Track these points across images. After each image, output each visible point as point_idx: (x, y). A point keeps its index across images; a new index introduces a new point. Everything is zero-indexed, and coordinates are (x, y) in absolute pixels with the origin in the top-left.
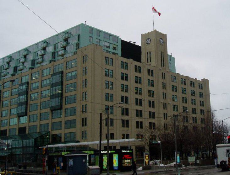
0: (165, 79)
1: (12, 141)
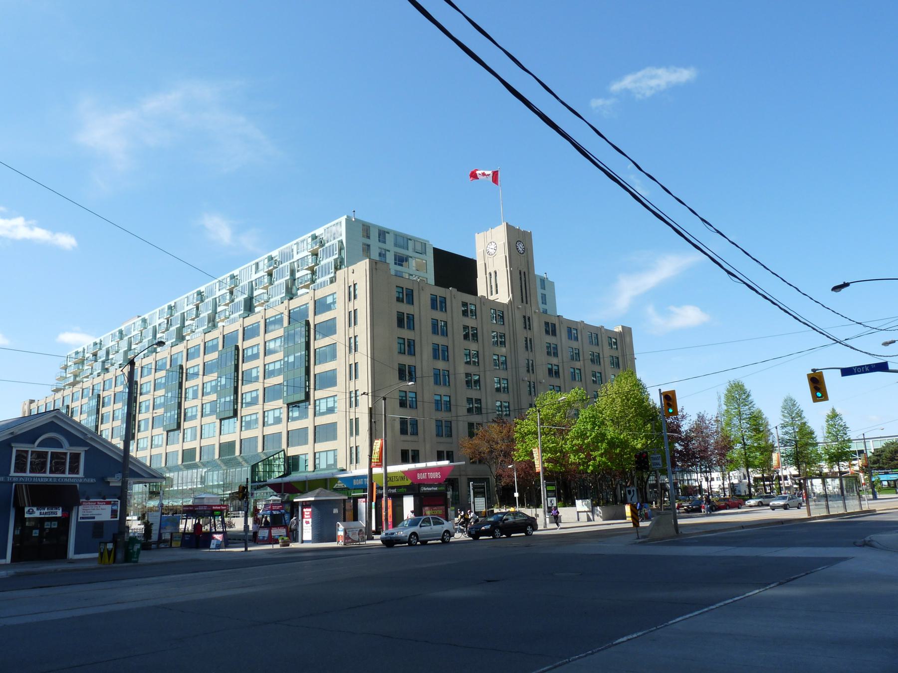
0: (530, 329)
1: (205, 472)
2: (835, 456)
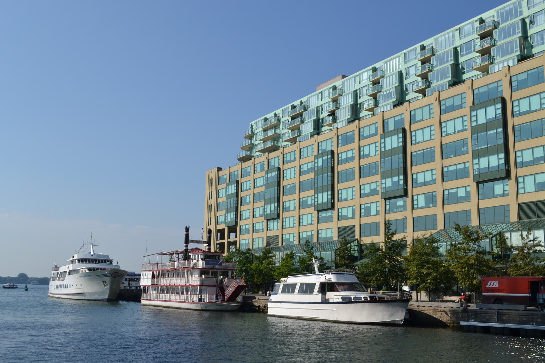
2: (444, 273)
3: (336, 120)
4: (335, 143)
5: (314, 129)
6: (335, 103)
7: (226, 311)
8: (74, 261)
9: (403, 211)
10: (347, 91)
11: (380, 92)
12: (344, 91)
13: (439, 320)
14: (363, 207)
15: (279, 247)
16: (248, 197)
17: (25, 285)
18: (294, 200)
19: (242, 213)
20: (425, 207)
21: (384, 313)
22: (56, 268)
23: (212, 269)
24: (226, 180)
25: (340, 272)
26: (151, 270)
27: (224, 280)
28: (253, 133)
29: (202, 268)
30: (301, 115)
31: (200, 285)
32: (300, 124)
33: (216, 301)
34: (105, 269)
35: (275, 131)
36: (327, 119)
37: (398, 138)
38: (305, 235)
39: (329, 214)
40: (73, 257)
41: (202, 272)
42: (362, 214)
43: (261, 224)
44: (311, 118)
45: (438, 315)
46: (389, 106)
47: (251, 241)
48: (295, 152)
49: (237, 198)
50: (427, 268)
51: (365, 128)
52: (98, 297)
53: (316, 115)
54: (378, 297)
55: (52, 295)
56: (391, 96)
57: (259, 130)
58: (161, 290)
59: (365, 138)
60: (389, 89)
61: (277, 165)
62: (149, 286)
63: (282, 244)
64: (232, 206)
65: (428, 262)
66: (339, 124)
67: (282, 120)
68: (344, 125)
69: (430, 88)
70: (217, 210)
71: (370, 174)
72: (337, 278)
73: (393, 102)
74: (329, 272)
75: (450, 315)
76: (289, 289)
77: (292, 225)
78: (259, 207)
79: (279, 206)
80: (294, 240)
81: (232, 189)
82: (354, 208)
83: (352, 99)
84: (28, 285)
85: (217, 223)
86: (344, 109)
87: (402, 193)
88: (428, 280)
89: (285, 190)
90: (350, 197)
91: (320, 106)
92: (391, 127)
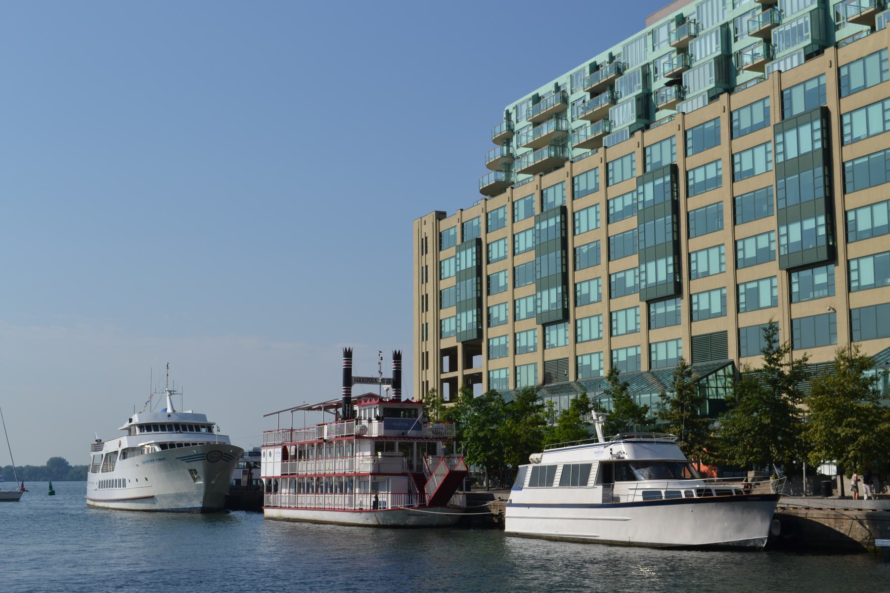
3: (684, 93)
4: (679, 148)
5: (638, 117)
6: (769, 10)
7: (430, 527)
8: (132, 428)
9: (828, 296)
10: (708, 27)
11: (778, 25)
12: (700, 26)
13: (847, 537)
14: (742, 289)
15: (569, 384)
16: (502, 275)
17: (20, 483)
18: (597, 278)
19: (491, 312)
20: (874, 286)
21: (726, 524)
22: (98, 445)
23: (399, 438)
24: (455, 239)
25: (642, 439)
26: (279, 445)
27: (426, 462)
28: (510, 130)
29: (379, 437)
30: (610, 85)
31: (371, 474)
32: (607, 107)
33: (409, 507)
34: (196, 444)
35: (557, 124)
36: (664, 93)
37: (813, 131)
38: (622, 356)
39: (671, 307)
40: (131, 420)
41: (379, 445)
42: (742, 306)
43: (531, 334)
44: (631, 92)
45: (844, 528)
46: (795, 58)
47: (511, 371)
48: (597, 170)
49: (479, 278)
50: (848, 425)
51: (742, 112)
52: (184, 504)
53: (641, 84)
54: (716, 490)
55: (92, 503)
56: (801, 34)
57: (522, 124)
58: (303, 485)
59: (743, 133)
60: (797, 19)
61: (559, 203)
62: (276, 479)
63: (577, 377)
64: (469, 297)
65: (852, 412)
66: (690, 103)
67: (572, 99)
68: (701, 105)
69: (884, 12)
70: (440, 305)
71: (757, 216)
72: (635, 452)
73: (805, 48)
74: (620, 439)
75: (867, 527)
76: (543, 477)
77: (595, 335)
78: (526, 297)
79: (565, 293)
80: (600, 369)
81: (468, 259)
82: (724, 291)
83: (717, 43)
84: (31, 483)
85: (440, 335)
86: (701, 69)
87: (824, 256)
88: (849, 452)
89: (578, 258)
90: (714, 269)
91: (651, 63)
92: (798, 106)
